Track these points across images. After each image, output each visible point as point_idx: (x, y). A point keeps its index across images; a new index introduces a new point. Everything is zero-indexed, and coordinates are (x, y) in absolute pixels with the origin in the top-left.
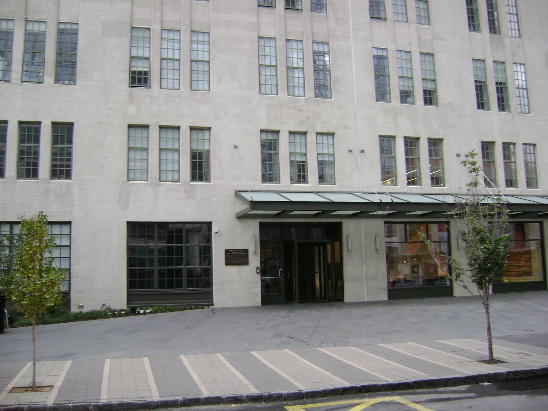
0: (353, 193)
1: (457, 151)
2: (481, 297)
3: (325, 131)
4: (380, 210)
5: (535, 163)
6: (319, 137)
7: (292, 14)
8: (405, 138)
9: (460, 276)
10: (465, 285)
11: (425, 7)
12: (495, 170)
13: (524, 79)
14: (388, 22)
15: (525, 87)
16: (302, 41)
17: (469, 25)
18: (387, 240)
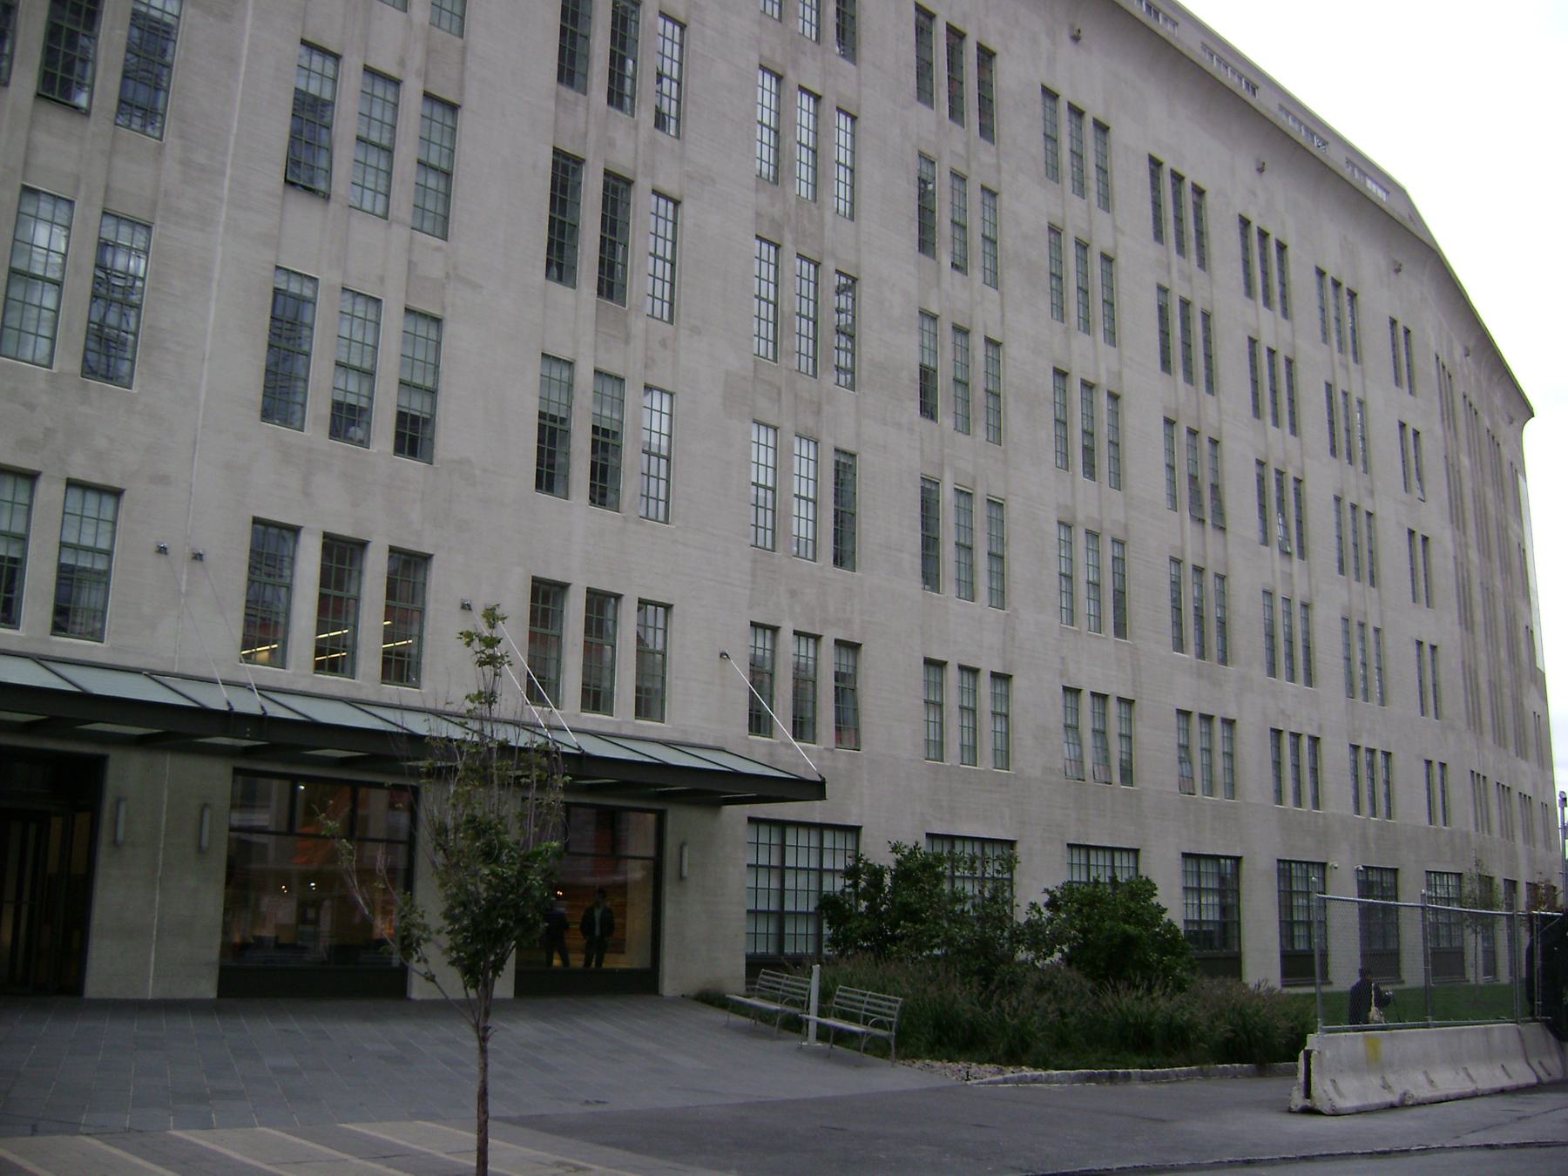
0: (152, 675)
1: (466, 596)
2: (466, 1004)
3: (96, 479)
4: (225, 734)
5: (664, 656)
6: (76, 494)
7: (56, 118)
8: (326, 536)
9: (419, 945)
10: (435, 972)
11: (442, 187)
12: (559, 661)
13: (665, 430)
14: (332, 205)
15: (664, 452)
16: (71, 203)
17: (549, 263)
18: (237, 818)
